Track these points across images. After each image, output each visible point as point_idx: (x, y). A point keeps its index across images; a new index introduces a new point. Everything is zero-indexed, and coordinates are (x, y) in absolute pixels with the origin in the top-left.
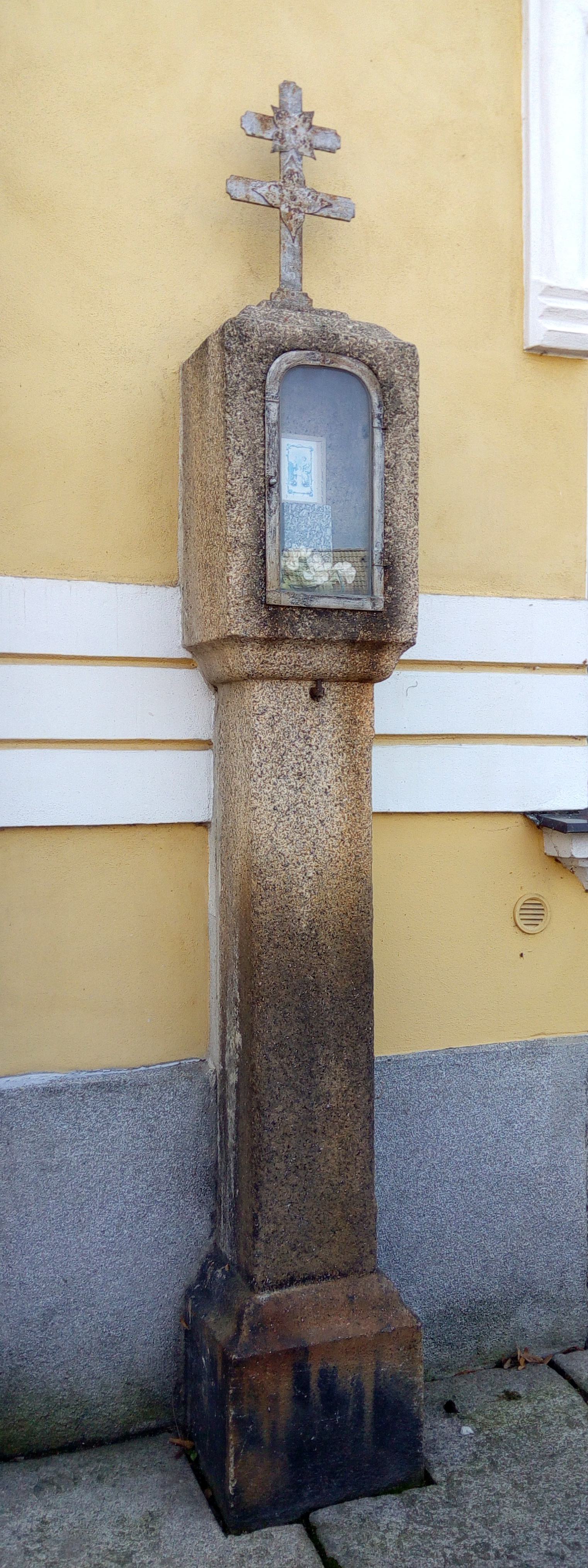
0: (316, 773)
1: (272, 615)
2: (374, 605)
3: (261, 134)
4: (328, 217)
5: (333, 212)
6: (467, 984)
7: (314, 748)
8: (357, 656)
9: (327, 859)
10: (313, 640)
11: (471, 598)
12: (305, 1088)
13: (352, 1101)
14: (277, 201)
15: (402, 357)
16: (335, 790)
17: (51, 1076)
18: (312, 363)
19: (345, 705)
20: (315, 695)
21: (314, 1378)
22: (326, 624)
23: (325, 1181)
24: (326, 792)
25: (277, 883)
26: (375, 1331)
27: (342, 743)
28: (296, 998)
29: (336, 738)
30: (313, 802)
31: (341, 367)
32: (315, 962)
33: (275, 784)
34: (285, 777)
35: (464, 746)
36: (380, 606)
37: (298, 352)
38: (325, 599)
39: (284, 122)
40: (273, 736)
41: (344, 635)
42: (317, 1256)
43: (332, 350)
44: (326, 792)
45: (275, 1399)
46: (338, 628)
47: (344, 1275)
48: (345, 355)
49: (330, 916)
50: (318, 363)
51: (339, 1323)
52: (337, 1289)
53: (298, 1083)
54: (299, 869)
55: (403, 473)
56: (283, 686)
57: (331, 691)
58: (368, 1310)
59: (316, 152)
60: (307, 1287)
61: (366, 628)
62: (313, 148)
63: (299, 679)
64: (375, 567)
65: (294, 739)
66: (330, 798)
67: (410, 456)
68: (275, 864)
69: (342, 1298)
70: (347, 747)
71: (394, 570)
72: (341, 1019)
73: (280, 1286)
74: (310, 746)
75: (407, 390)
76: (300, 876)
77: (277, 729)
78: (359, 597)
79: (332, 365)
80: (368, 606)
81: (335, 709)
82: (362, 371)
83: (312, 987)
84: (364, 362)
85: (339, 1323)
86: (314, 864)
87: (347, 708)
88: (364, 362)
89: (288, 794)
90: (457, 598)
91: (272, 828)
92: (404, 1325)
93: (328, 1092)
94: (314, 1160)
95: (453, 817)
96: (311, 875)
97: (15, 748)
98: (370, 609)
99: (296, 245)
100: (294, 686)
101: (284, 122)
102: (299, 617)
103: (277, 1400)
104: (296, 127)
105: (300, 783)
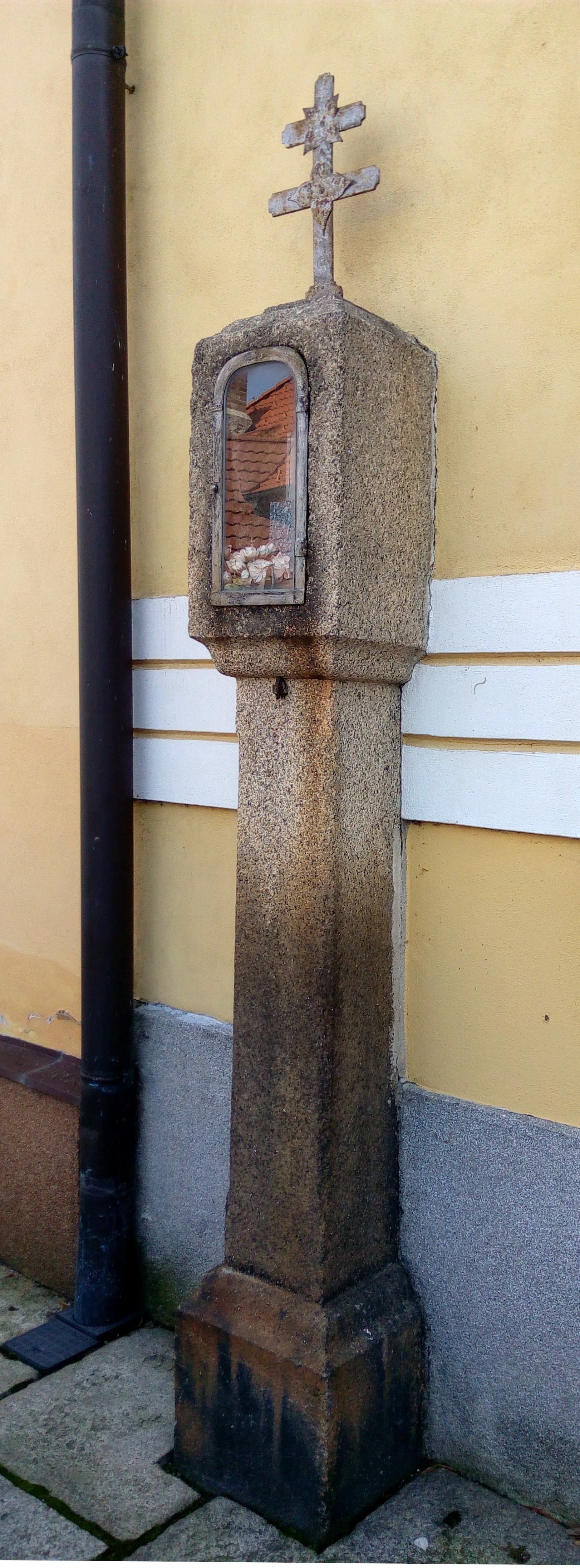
0: (281, 772)
1: (218, 614)
2: (295, 598)
3: (297, 142)
4: (355, 195)
5: (357, 187)
6: (502, 1033)
7: (280, 746)
8: (296, 652)
9: (288, 859)
10: (249, 638)
11: (545, 576)
12: (265, 1084)
13: (304, 1114)
14: (307, 201)
15: (326, 329)
16: (296, 790)
17: (215, 1022)
18: (248, 363)
19: (307, 703)
20: (281, 692)
21: (234, 1369)
22: (258, 621)
23: (280, 1186)
24: (289, 791)
25: (249, 876)
26: (285, 1356)
27: (303, 742)
28: (261, 993)
29: (298, 737)
30: (278, 800)
31: (271, 359)
32: (277, 961)
33: (250, 779)
34: (258, 773)
35: (537, 754)
36: (300, 599)
37: (239, 356)
38: (255, 596)
39: (313, 119)
40: (249, 733)
41: (272, 631)
42: (271, 1258)
43: (266, 344)
44: (289, 791)
45: (205, 1367)
46: (268, 625)
47: (294, 1290)
48: (277, 345)
49: (289, 917)
50: (253, 361)
51: (264, 1329)
52: (279, 1298)
53: (260, 1076)
54: (266, 865)
55: (325, 454)
56: (258, 684)
57: (295, 687)
58: (292, 1334)
59: (342, 134)
60: (261, 1283)
61: (292, 623)
62: (338, 130)
63: (266, 676)
64: (297, 559)
65: (265, 736)
66: (293, 798)
67: (330, 433)
68: (247, 857)
69: (277, 1309)
70: (307, 747)
71: (315, 560)
72: (296, 1026)
73: (243, 1269)
74: (277, 743)
75: (329, 364)
76: (267, 872)
77: (253, 726)
78: (283, 591)
79: (264, 360)
80: (290, 600)
81: (298, 707)
82: (289, 357)
83: (273, 986)
84: (292, 347)
85: (264, 1329)
86: (277, 862)
87: (308, 706)
88: (292, 347)
89: (259, 790)
90: (530, 576)
91: (246, 822)
92: (311, 1367)
93: (284, 1096)
94: (270, 1160)
95: (535, 840)
96: (275, 873)
97: (189, 738)
98: (292, 603)
99: (326, 237)
100: (265, 681)
101: (313, 119)
102: (238, 615)
103: (325, 1400)
104: (324, 118)
105: (269, 779)
